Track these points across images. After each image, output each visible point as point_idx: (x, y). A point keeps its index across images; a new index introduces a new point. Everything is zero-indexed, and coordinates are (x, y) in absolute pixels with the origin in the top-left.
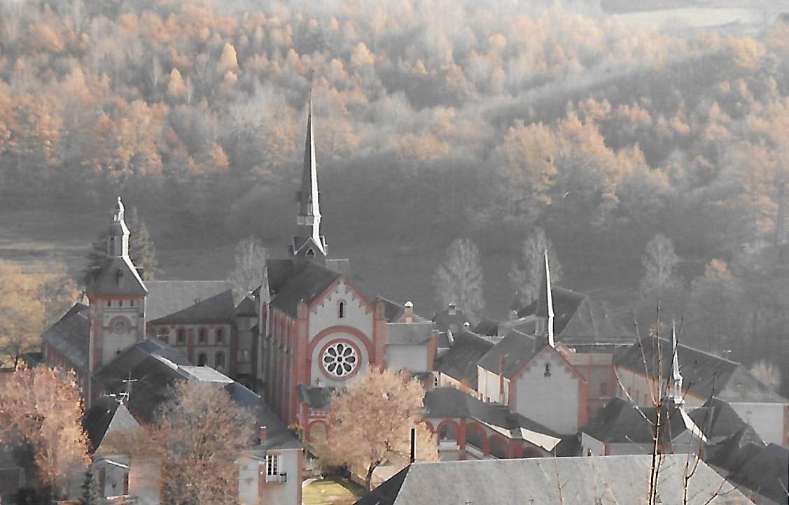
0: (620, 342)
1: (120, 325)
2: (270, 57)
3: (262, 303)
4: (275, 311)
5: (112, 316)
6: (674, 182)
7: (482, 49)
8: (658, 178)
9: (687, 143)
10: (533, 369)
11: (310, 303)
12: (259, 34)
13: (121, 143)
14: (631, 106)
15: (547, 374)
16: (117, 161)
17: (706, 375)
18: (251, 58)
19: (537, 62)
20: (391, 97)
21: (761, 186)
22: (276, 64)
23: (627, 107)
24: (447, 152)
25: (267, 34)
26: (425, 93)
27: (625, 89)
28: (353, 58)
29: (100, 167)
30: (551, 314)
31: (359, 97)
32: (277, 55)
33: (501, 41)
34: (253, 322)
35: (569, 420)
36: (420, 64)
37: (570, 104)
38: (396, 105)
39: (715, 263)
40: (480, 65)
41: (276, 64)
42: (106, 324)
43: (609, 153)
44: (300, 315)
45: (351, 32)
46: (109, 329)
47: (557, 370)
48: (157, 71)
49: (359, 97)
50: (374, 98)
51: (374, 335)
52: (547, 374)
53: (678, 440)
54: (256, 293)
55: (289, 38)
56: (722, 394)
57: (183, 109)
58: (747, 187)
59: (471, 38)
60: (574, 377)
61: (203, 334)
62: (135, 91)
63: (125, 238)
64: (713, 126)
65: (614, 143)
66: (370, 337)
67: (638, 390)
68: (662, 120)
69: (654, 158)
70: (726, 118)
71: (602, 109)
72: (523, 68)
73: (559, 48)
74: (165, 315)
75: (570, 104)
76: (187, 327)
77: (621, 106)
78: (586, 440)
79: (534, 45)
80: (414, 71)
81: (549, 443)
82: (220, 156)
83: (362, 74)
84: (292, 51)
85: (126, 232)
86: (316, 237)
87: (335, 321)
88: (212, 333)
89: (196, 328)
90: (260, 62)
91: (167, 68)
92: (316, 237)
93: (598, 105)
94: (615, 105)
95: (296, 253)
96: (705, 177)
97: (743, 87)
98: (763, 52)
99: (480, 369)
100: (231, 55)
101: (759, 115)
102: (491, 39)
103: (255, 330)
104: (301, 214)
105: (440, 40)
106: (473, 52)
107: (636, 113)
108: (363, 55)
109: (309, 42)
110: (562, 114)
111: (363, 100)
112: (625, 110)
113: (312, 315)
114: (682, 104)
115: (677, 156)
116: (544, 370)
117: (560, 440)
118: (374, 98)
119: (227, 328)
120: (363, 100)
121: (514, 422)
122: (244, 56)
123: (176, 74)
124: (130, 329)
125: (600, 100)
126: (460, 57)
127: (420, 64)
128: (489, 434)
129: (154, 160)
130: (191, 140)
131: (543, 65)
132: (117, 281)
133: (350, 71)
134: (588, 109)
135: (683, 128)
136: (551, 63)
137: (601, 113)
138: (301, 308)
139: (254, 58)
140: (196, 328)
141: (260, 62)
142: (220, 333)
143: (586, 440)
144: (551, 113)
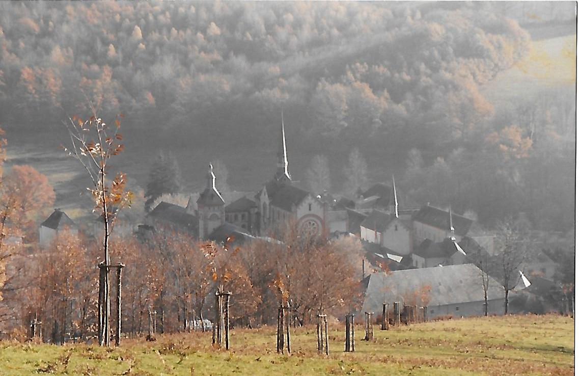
0: (414, 209)
1: (214, 217)
2: (160, 33)
3: (262, 204)
4: (272, 207)
5: (211, 214)
6: (408, 110)
7: (282, 24)
8: (400, 109)
9: (412, 86)
10: (304, 204)
11: (297, 205)
12: (151, 18)
13: (96, 93)
14: (379, 66)
15: (396, 230)
16: (94, 103)
17: (463, 226)
18: (150, 34)
19: (312, 29)
20: (236, 57)
21: (454, 114)
22: (165, 37)
23: (377, 67)
24: (287, 98)
25: (155, 17)
26: (254, 52)
27: (373, 55)
28: (208, 31)
29: (85, 107)
30: (397, 204)
31: (217, 56)
32: (165, 31)
33: (290, 17)
34: (256, 210)
35: (406, 250)
36: (248, 34)
37: (347, 67)
38: (240, 62)
39: (439, 159)
40: (282, 33)
41: (165, 37)
42: (209, 217)
43: (375, 97)
44: (293, 210)
45: (204, 15)
46: (210, 219)
47: (400, 228)
48: (99, 46)
49: (217, 56)
50: (226, 57)
51: (324, 217)
52: (396, 230)
53: (455, 256)
54: (258, 197)
55: (169, 20)
56: (468, 233)
57: (120, 68)
58: (447, 114)
59: (273, 17)
60: (407, 230)
61: (236, 217)
62: (89, 58)
63: (214, 180)
64: (424, 78)
65: (375, 89)
66: (322, 217)
67: (436, 234)
68: (397, 75)
69: (396, 98)
70: (429, 71)
71: (362, 68)
72: (306, 34)
73: (324, 21)
74: (166, 202)
75: (347, 67)
76: (230, 214)
77: (373, 66)
78: (415, 257)
79: (310, 19)
80: (245, 39)
81: (399, 259)
82: (150, 98)
83: (215, 42)
84: (173, 29)
85: (214, 177)
86: (286, 173)
87: (308, 212)
88: (240, 216)
89: (233, 214)
90: (155, 36)
91: (106, 43)
92: (286, 173)
93: (362, 67)
94: (370, 64)
95: (278, 180)
96: (426, 107)
97: (436, 53)
98: (444, 31)
99: (362, 228)
100: (138, 32)
101: (446, 69)
102: (285, 17)
103: (258, 214)
104: (279, 162)
105: (255, 17)
106: (277, 26)
107: (381, 70)
108: (214, 29)
109: (181, 23)
110: (344, 72)
111: (220, 58)
112: (376, 68)
113: (298, 210)
114: (405, 64)
115: (409, 95)
116: (394, 228)
117: (402, 258)
118: (226, 57)
119: (246, 213)
120: (220, 58)
121: (384, 251)
122: (146, 31)
123: (112, 47)
124: (218, 219)
125: (362, 63)
126: (270, 28)
127: (248, 34)
128: (374, 256)
129: (115, 102)
130: (128, 87)
131: (316, 31)
132: (212, 199)
133: (208, 39)
134: (357, 69)
135: (407, 78)
136: (321, 30)
137: (364, 70)
138: (293, 209)
139: (152, 33)
140: (233, 214)
141: (155, 36)
142: (243, 216)
143: (415, 257)
144: (336, 71)
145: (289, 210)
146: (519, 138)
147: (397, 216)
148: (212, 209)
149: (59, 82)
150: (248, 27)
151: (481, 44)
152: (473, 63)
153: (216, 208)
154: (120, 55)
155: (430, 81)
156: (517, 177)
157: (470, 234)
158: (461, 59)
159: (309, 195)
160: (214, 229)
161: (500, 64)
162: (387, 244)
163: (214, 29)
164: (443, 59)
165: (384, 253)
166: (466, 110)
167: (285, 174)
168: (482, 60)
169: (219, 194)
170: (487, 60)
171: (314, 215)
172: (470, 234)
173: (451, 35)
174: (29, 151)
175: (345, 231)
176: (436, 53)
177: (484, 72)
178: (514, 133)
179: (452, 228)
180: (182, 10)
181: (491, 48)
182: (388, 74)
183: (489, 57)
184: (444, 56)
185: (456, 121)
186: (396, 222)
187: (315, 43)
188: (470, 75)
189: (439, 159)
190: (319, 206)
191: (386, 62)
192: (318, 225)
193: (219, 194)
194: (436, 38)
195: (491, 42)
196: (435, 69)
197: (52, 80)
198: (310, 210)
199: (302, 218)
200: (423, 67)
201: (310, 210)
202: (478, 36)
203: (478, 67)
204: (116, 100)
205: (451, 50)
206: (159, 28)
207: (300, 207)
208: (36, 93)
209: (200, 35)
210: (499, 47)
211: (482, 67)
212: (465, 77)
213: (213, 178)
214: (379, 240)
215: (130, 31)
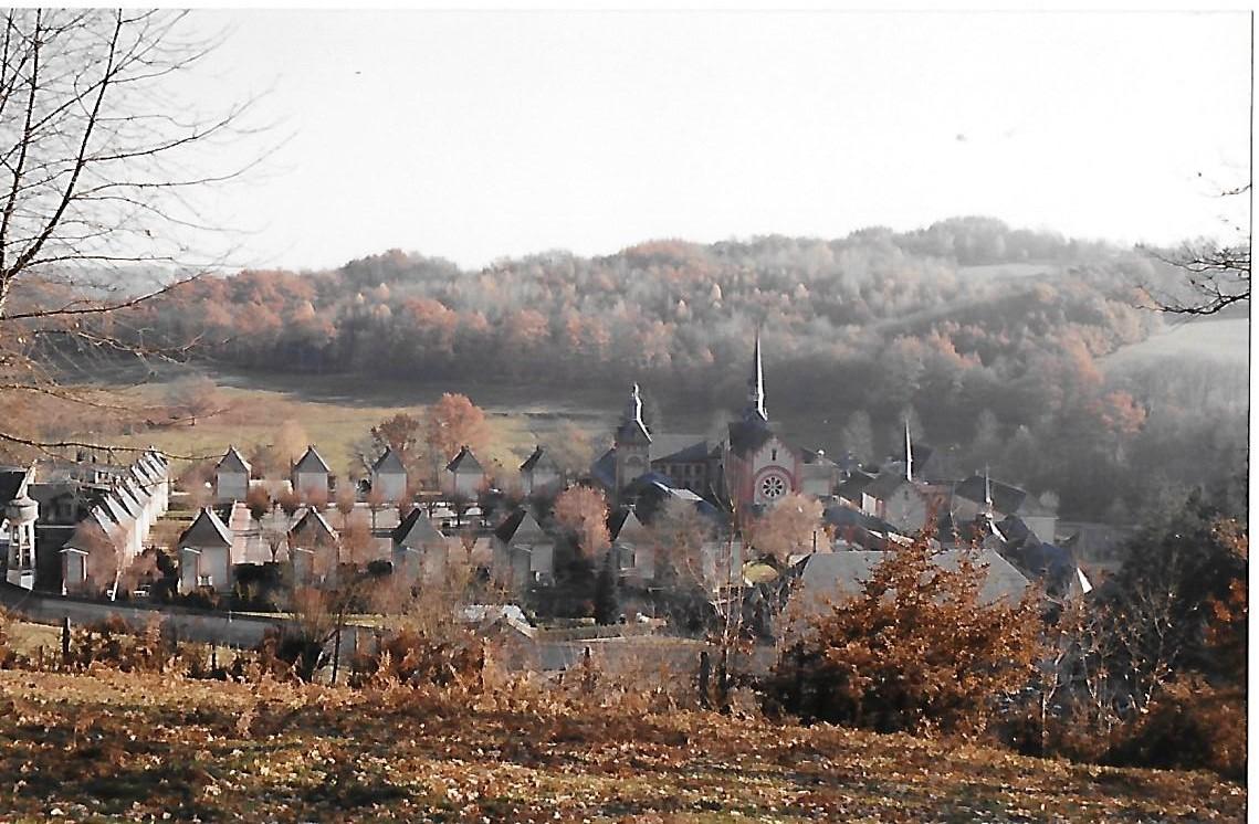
2: (742, 293)
5: (630, 456)
27: (969, 315)
31: (799, 318)
32: (747, 291)
39: (1022, 427)
40: (877, 298)
64: (1025, 341)
66: (792, 471)
68: (993, 336)
69: (987, 361)
70: (1033, 335)
72: (906, 300)
79: (913, 286)
82: (709, 356)
87: (770, 462)
88: (693, 468)
92: (760, 408)
96: (1019, 372)
97: (1044, 316)
101: (1053, 334)
108: (802, 292)
112: (969, 328)
113: (755, 459)
118: (809, 319)
119: (703, 465)
121: (884, 529)
124: (641, 465)
126: (865, 293)
130: (685, 343)
133: (793, 301)
135: (1005, 341)
138: (749, 453)
141: (735, 296)
145: (743, 457)
146: (1128, 407)
147: (909, 477)
148: (631, 449)
149: (608, 335)
150: (842, 291)
151: (1099, 309)
152: (1087, 330)
153: (639, 449)
154: (691, 314)
155: (1031, 345)
156: (1120, 455)
157: (1020, 512)
158: (1073, 324)
159: (775, 436)
160: (634, 480)
161: (1122, 335)
162: (891, 519)
163: (802, 292)
164: (1052, 322)
165: (884, 532)
166: (1067, 378)
167: (758, 412)
168: (1099, 328)
169: (645, 430)
170: (1106, 329)
171: (778, 468)
172: (1020, 512)
173: (1065, 298)
174: (565, 406)
175: (827, 495)
176: (1044, 316)
177: (1102, 341)
178: (1122, 402)
179: (988, 500)
180: (771, 272)
181: (1112, 316)
182: (984, 335)
183: (1109, 326)
184: (1053, 318)
185: (1055, 388)
186: (906, 487)
187: (913, 309)
188: (1081, 341)
189: (1022, 427)
190: (789, 454)
191: (983, 323)
192: (777, 475)
193: (645, 430)
194: (1045, 299)
195: (1112, 309)
196: (1039, 333)
197: (602, 332)
198: (774, 459)
199: (760, 472)
200: (1026, 330)
201: (774, 459)
202: (1096, 300)
203: (1094, 335)
204: (669, 357)
205: (1062, 313)
206: (741, 287)
207: (759, 453)
208: (580, 344)
209: (785, 297)
210: (1121, 316)
211: (1099, 336)
212: (1076, 343)
213: (636, 405)
214: (880, 512)
215: (709, 290)
